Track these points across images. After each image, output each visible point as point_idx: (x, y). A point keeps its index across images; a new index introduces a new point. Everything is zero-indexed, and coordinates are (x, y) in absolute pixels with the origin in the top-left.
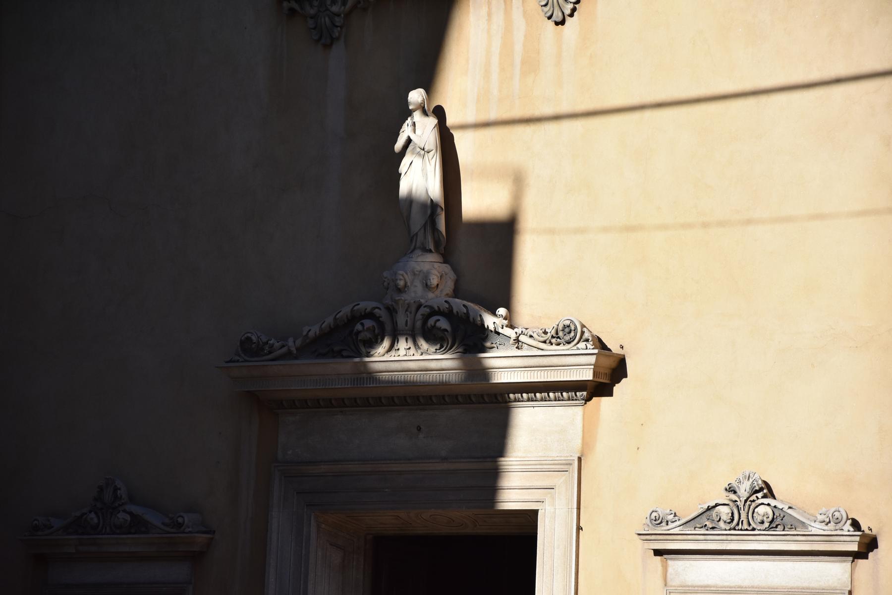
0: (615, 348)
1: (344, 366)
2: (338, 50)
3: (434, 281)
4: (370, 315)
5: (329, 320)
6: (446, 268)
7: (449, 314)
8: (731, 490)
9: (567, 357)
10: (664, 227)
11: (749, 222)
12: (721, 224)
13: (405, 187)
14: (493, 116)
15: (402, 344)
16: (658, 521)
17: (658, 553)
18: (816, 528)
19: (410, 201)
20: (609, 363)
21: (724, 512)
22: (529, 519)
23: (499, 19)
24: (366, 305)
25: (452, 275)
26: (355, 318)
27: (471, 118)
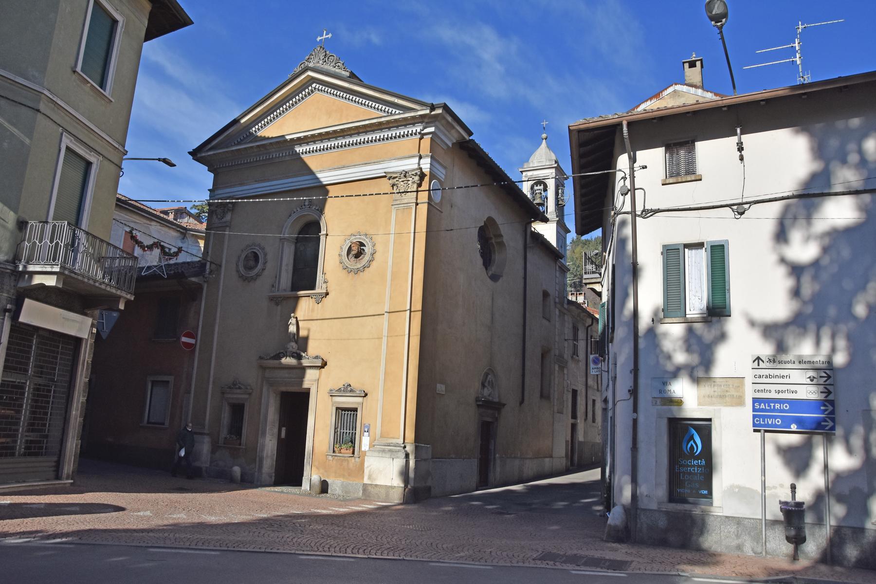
0: (325, 360)
1: (276, 362)
2: (279, 307)
3: (294, 347)
4: (282, 353)
5: (275, 354)
6: (296, 345)
7: (296, 353)
8: (344, 385)
9: (522, 304)
10: (334, 339)
11: (349, 339)
12: (344, 339)
13: (290, 330)
14: (306, 319)
15: (288, 358)
16: (331, 390)
17: (331, 396)
18: (358, 392)
19: (290, 333)
20: (324, 363)
21: (342, 389)
22: (309, 389)
23: (307, 303)
24: (282, 351)
25: (297, 346)
26: (279, 353)
27: (302, 319)
